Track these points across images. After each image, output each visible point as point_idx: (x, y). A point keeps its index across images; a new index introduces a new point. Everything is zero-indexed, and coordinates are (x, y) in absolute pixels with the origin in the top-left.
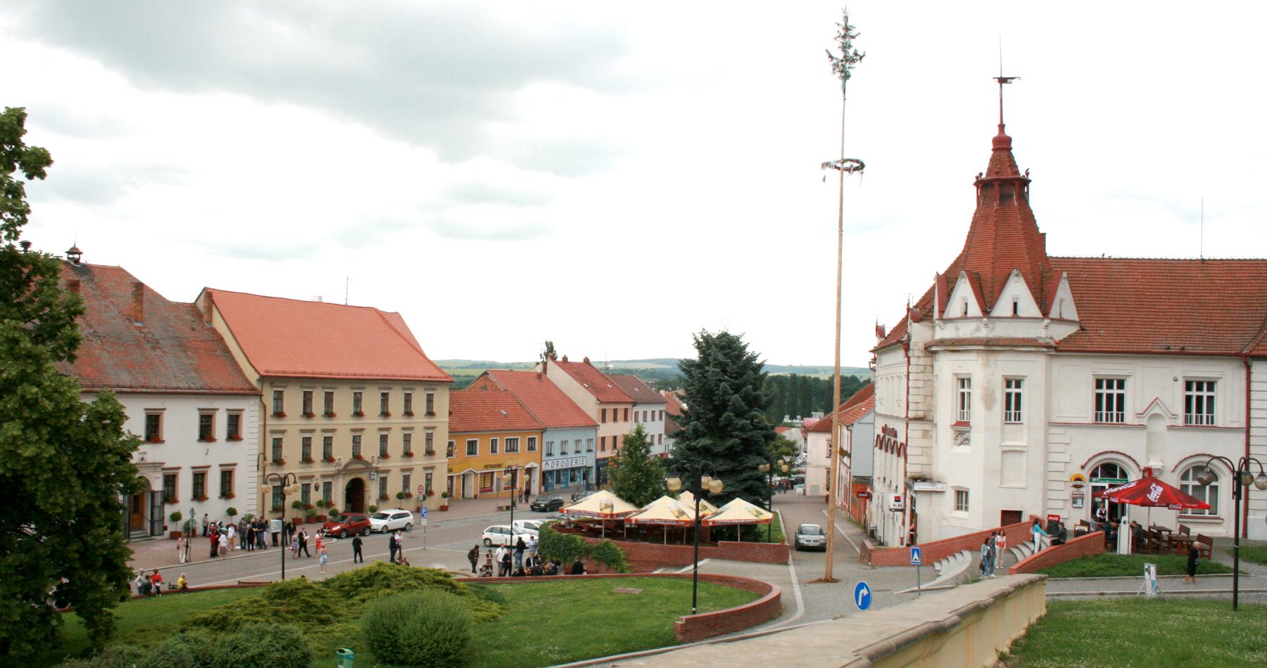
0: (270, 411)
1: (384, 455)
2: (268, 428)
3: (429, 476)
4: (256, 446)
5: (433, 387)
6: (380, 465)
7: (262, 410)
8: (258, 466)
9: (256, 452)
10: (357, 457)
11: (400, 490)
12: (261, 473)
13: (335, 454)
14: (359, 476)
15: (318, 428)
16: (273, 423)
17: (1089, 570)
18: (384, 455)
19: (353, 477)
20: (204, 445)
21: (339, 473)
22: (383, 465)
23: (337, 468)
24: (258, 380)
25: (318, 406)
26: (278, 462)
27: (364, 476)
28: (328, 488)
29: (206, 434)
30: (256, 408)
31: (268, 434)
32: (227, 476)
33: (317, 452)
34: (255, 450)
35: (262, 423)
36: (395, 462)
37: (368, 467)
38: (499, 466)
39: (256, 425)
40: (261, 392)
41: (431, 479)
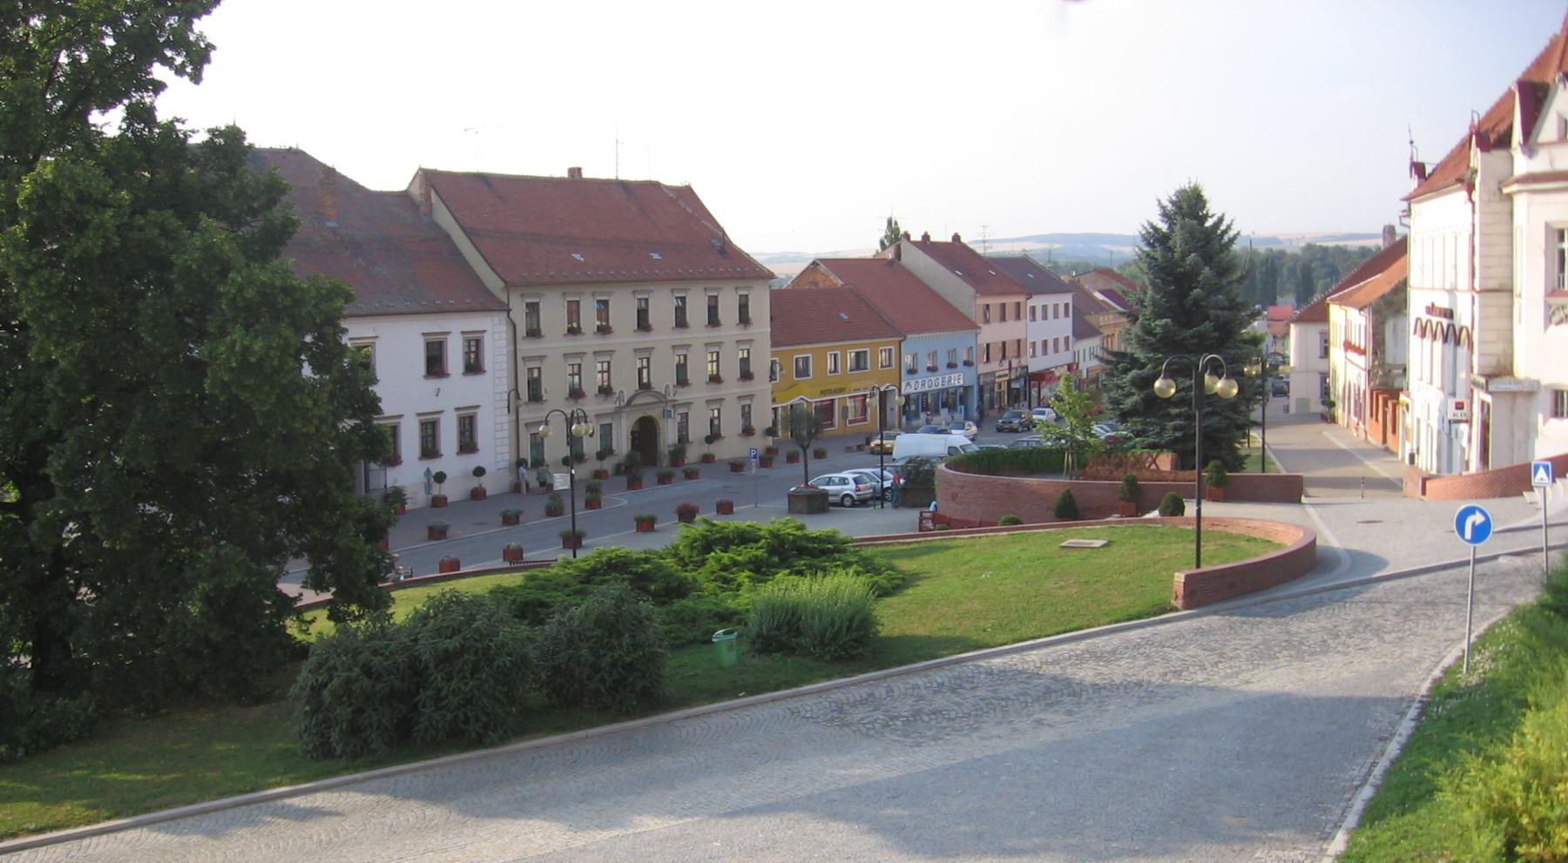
0: (522, 330)
1: (682, 381)
2: (520, 355)
3: (747, 409)
4: (505, 381)
5: (605, 289)
6: (676, 398)
7: (511, 328)
8: (509, 407)
9: (505, 389)
10: (645, 387)
11: (566, 452)
12: (514, 417)
13: (616, 388)
14: (650, 413)
15: (590, 351)
16: (527, 347)
17: (1278, 658)
18: (682, 381)
19: (641, 415)
20: (435, 383)
21: (618, 412)
22: (682, 395)
23: (618, 405)
24: (502, 289)
25: (589, 319)
26: (535, 396)
27: (655, 413)
28: (606, 431)
29: (435, 365)
30: (503, 327)
31: (520, 363)
32: (467, 426)
33: (731, 371)
34: (504, 385)
35: (512, 348)
36: (698, 392)
37: (662, 398)
38: (841, 391)
39: (504, 351)
40: (508, 305)
41: (749, 413)
